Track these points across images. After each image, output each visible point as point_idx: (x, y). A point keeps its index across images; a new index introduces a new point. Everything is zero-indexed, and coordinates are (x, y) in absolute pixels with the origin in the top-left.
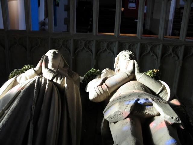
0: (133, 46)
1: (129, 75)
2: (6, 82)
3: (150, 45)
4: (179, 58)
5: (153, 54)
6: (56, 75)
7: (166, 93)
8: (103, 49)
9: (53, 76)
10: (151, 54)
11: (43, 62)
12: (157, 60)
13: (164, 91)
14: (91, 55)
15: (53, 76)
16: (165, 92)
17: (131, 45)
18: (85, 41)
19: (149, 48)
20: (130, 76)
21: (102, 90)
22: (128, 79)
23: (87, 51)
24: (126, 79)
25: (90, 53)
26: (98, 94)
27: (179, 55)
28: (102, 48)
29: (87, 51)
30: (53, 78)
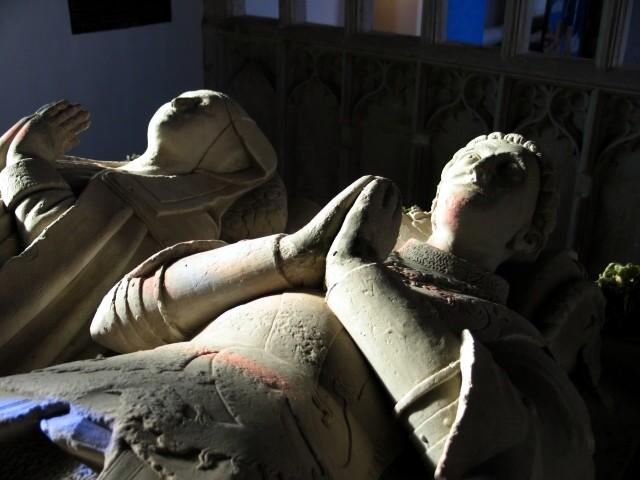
1: (285, 256)
3: (552, 89)
6: (34, 188)
7: (446, 421)
8: (631, 133)
9: (17, 190)
11: (29, 122)
13: (435, 405)
14: (575, 154)
15: (20, 191)
16: (444, 415)
18: (555, 88)
20: (290, 260)
21: (138, 301)
22: (280, 280)
23: (561, 137)
24: (262, 273)
25: (574, 144)
26: (116, 316)
29: (561, 137)
30: (16, 201)
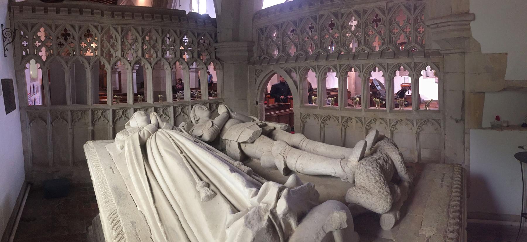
0: (105, 112)
2: (280, 3)
3: (180, 107)
4: (170, 118)
5: (166, 116)
10: (182, 114)
12: (188, 118)
17: (164, 109)
18: (81, 111)
19: (180, 110)
27: (108, 119)
28: (118, 116)
